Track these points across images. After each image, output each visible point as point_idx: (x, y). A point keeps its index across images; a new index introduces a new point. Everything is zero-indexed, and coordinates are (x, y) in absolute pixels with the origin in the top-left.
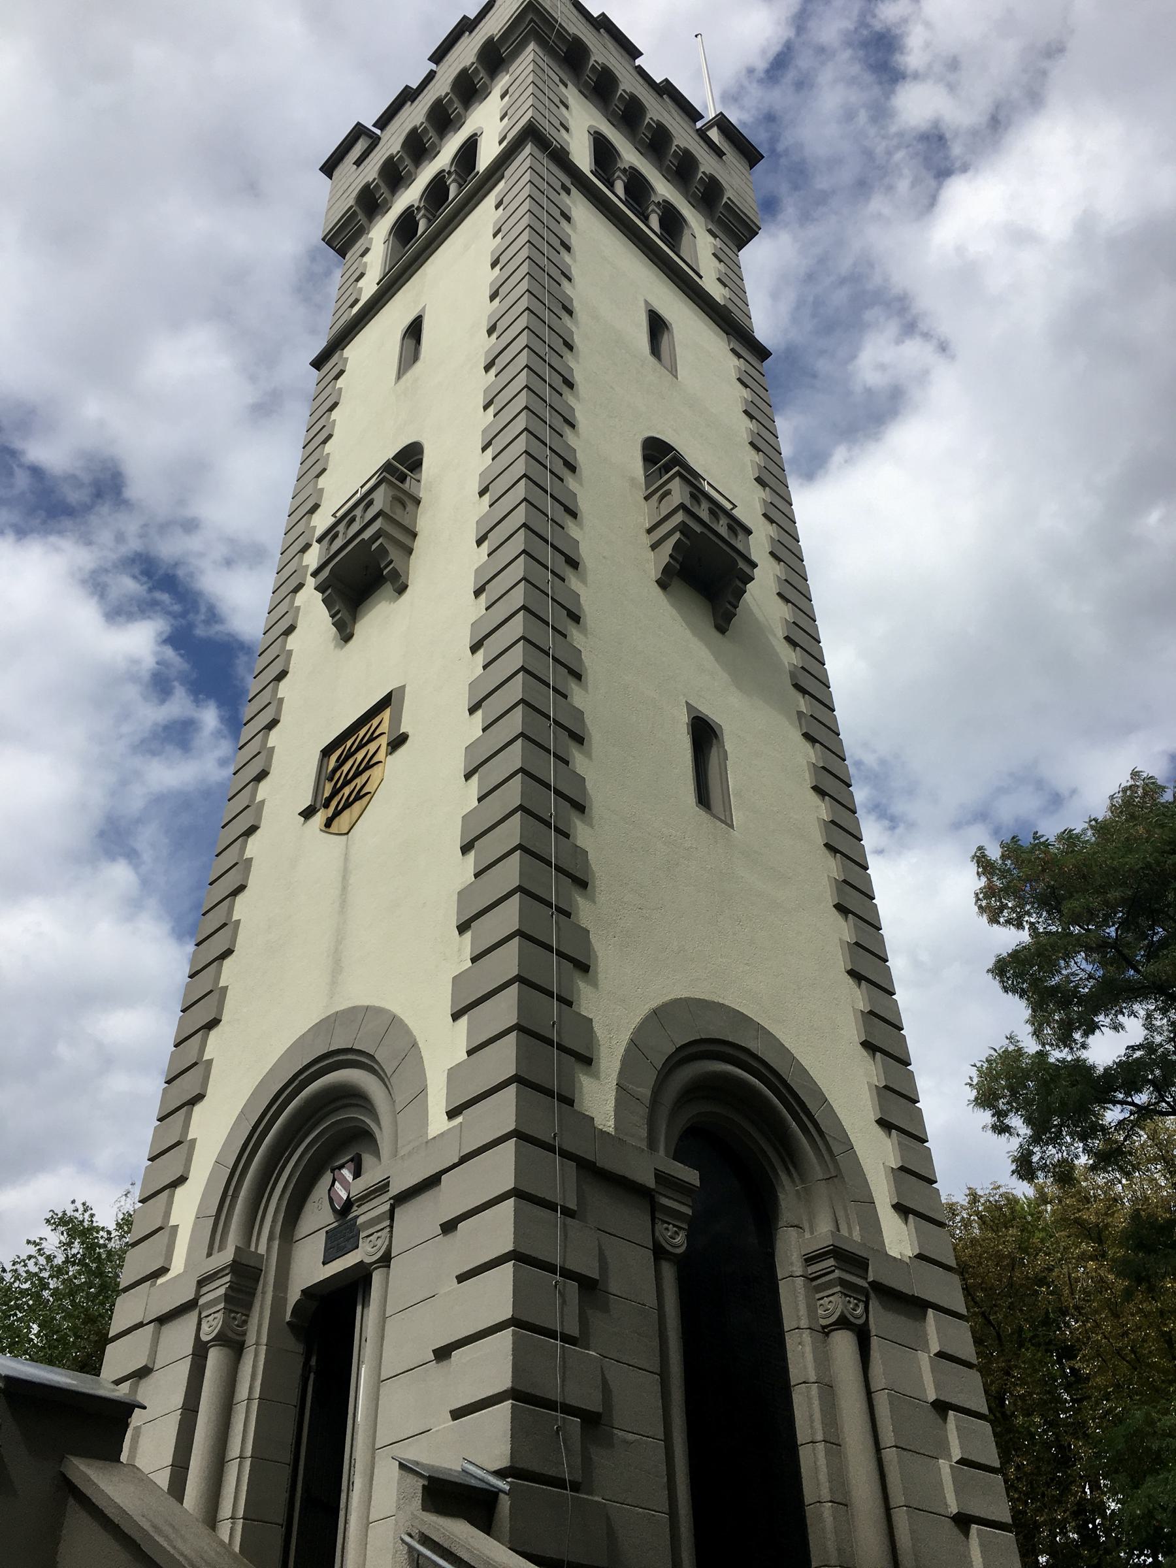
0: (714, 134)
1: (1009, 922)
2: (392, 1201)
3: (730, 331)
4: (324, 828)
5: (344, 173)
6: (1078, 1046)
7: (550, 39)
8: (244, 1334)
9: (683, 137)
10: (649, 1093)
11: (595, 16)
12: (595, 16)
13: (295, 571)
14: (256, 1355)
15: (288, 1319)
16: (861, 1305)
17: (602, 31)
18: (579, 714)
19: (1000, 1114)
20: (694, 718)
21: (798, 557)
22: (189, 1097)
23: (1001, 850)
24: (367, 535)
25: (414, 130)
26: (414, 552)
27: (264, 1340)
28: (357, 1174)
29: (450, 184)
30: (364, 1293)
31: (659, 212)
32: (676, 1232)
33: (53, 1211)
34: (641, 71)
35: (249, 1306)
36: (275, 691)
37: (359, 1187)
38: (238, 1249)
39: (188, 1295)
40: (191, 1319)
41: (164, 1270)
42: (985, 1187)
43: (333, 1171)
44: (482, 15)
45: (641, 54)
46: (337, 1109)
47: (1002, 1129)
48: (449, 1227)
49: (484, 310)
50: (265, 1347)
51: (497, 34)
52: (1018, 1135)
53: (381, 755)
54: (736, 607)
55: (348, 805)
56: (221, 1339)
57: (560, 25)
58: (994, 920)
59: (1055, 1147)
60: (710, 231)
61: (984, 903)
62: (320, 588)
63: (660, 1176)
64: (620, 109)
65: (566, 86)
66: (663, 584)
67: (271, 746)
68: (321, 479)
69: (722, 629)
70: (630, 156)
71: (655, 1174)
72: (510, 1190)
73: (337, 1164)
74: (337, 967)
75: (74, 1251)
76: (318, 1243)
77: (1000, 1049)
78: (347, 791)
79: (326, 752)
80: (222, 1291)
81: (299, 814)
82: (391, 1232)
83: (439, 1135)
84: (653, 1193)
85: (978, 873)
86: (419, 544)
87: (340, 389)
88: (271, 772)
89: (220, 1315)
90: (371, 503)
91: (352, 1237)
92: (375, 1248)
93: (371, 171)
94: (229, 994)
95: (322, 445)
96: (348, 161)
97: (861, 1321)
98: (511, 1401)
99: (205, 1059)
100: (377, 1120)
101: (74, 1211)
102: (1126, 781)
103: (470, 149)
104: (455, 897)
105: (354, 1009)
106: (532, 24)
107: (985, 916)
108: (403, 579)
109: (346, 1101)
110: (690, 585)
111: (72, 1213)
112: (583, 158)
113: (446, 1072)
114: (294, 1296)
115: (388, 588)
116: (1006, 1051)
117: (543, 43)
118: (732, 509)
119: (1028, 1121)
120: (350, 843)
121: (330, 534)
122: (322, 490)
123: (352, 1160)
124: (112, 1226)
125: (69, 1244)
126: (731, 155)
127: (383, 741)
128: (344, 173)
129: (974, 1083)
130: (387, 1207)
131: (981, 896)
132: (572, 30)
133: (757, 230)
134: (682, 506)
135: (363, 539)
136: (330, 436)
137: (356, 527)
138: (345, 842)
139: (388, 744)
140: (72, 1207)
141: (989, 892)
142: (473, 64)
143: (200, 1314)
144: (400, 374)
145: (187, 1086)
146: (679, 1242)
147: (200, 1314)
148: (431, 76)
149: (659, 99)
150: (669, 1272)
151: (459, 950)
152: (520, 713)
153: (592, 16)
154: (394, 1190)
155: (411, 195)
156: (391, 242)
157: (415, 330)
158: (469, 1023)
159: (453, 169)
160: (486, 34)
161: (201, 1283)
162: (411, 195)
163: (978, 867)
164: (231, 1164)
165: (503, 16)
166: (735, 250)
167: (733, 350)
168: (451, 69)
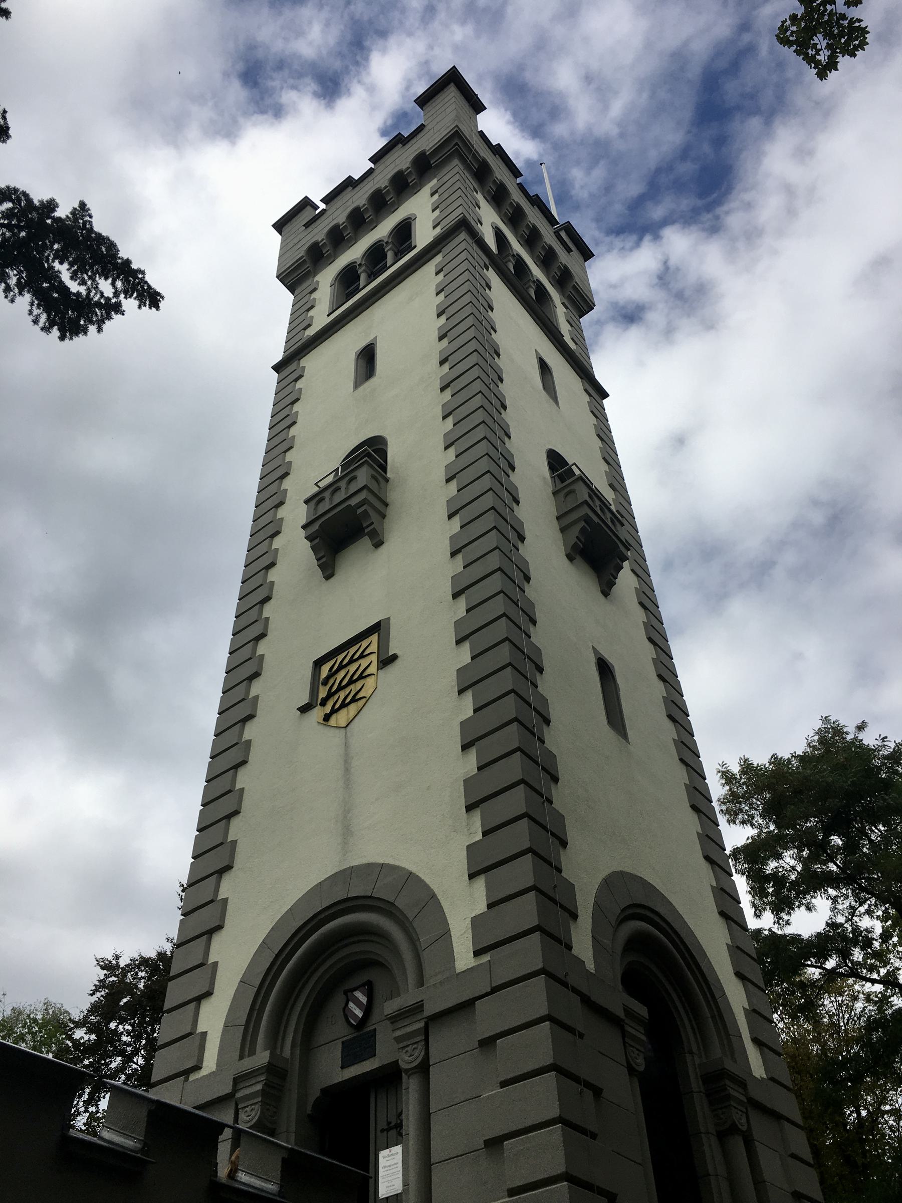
0: (563, 234)
1: (743, 822)
2: (426, 1020)
5: (293, 230)
6: (784, 923)
13: (271, 522)
16: (744, 1115)
17: (497, 156)
22: (208, 928)
24: (354, 502)
29: (387, 251)
31: (534, 287)
36: (261, 612)
39: (227, 1089)
41: (197, 1068)
44: (415, 134)
46: (346, 946)
48: (487, 1043)
51: (428, 150)
55: (344, 705)
57: (475, 150)
64: (510, 213)
65: (477, 193)
66: (570, 558)
68: (288, 454)
71: (624, 1008)
73: (347, 986)
74: (347, 832)
76: (337, 1052)
79: (318, 664)
80: (259, 1087)
81: (297, 709)
86: (390, 512)
89: (257, 1107)
90: (355, 478)
94: (240, 848)
95: (287, 429)
102: (819, 725)
103: (404, 231)
105: (369, 866)
106: (457, 146)
108: (381, 537)
109: (361, 938)
114: (315, 1093)
115: (366, 542)
117: (463, 160)
120: (349, 735)
123: (363, 985)
126: (575, 253)
127: (374, 658)
128: (293, 230)
130: (421, 1025)
133: (593, 306)
134: (365, 487)
135: (350, 505)
142: (408, 168)
143: (237, 1105)
147: (237, 1105)
148: (370, 172)
149: (532, 207)
153: (491, 144)
154: (430, 1009)
155: (355, 253)
159: (390, 241)
160: (419, 148)
162: (355, 253)
166: (578, 318)
167: (586, 390)
168: (389, 168)
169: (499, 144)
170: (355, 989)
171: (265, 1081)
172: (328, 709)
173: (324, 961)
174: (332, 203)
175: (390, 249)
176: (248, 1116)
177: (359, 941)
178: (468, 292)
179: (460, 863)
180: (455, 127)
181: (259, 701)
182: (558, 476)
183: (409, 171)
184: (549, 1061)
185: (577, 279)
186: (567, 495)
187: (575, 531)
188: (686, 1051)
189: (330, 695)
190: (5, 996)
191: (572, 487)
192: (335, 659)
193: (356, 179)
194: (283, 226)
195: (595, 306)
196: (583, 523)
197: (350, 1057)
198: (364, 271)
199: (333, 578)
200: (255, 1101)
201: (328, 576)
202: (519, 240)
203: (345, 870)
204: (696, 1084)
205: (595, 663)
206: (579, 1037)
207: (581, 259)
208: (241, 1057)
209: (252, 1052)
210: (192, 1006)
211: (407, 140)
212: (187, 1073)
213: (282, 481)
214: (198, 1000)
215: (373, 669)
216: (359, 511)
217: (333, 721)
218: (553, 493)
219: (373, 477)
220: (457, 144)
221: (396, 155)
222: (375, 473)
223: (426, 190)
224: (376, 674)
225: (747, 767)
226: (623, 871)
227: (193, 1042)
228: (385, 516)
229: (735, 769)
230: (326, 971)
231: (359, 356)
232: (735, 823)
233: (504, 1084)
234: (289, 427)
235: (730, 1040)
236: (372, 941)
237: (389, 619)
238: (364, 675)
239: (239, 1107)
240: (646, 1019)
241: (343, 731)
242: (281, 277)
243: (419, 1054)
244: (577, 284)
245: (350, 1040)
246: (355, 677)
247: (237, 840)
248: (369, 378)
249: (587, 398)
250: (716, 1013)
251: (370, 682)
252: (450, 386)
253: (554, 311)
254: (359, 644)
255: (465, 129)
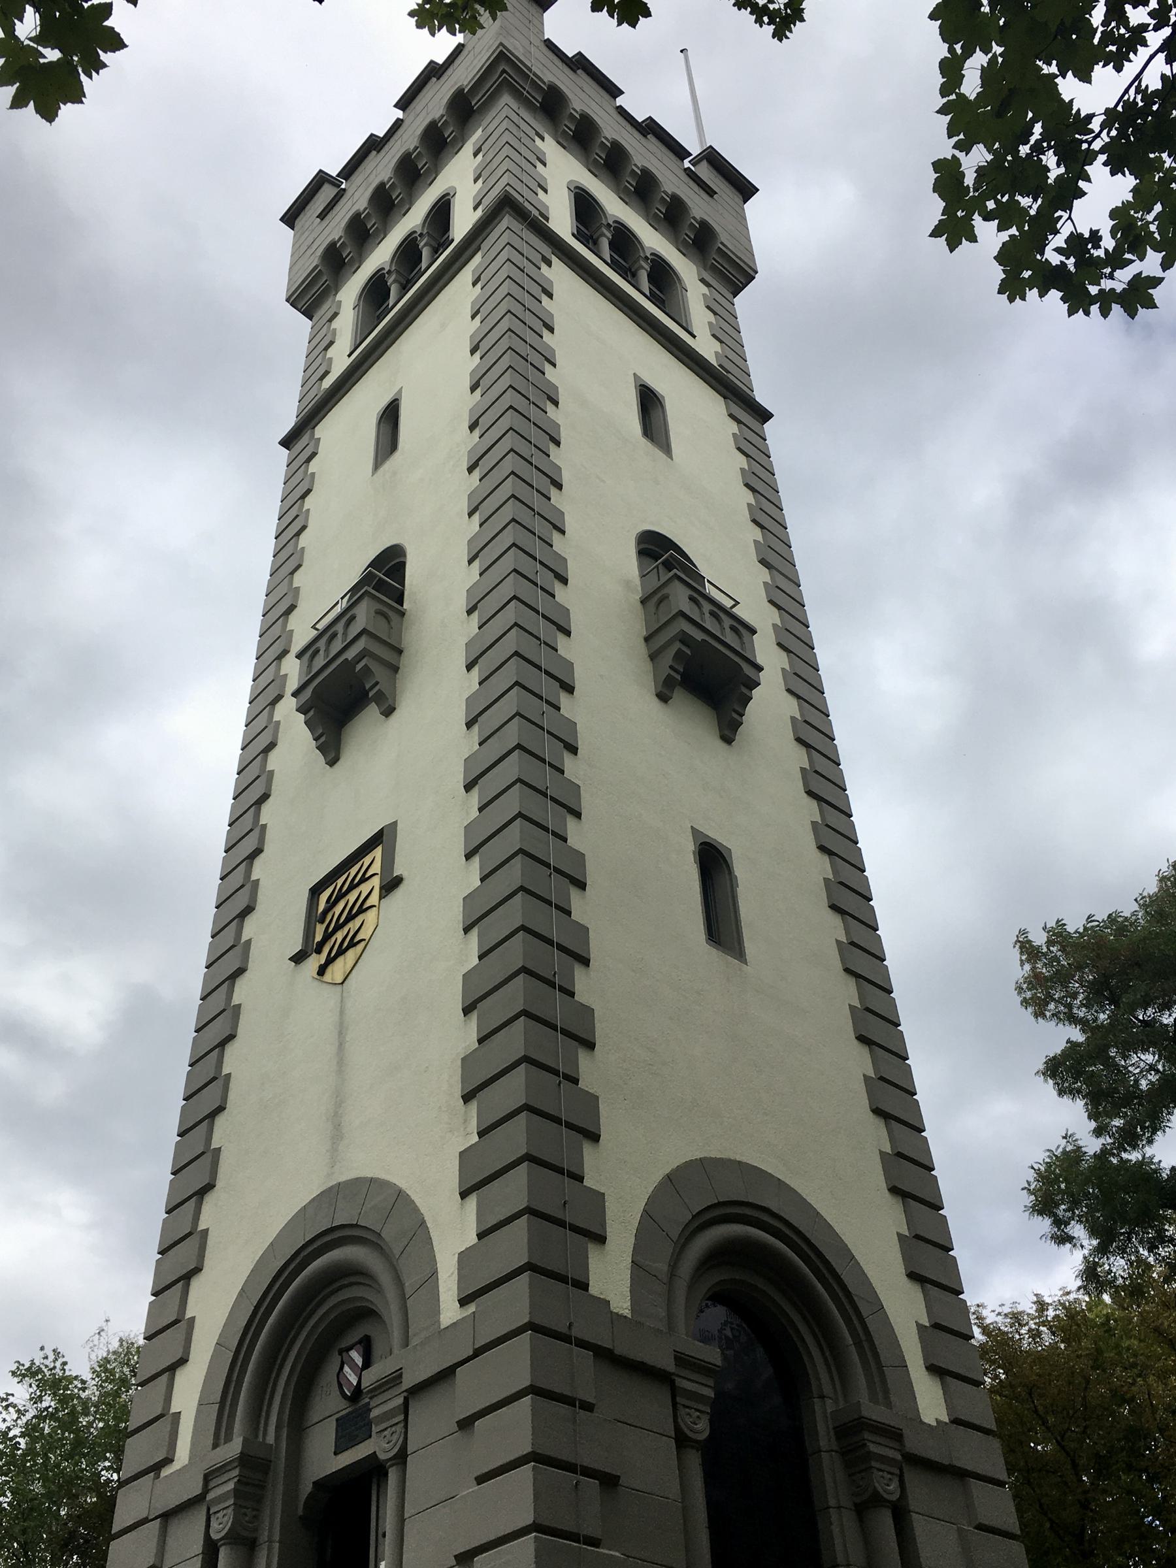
0: (704, 172)
2: (405, 1394)
3: (729, 395)
4: (316, 976)
7: (524, 89)
8: (256, 1530)
9: (671, 180)
10: (665, 1268)
11: (570, 56)
12: (570, 56)
14: (270, 1549)
15: (300, 1512)
17: (580, 71)
18: (580, 857)
19: (1058, 1222)
20: (701, 844)
21: (807, 645)
22: (185, 1271)
23: (1046, 934)
24: (351, 654)
25: (382, 185)
26: (400, 671)
27: (277, 1537)
28: (367, 1364)
30: (379, 1481)
32: (698, 1417)
33: (18, 1362)
34: (621, 111)
35: (259, 1500)
37: (370, 1377)
38: (246, 1442)
40: (198, 1518)
41: (169, 1461)
42: (1053, 1294)
43: (341, 1352)
45: (622, 93)
47: (1063, 1239)
48: (466, 1424)
49: (466, 402)
50: (278, 1544)
51: (467, 85)
52: (1082, 1246)
53: (374, 899)
54: (742, 715)
55: (341, 952)
56: (233, 1538)
57: (535, 74)
58: (1039, 1014)
59: (1123, 1258)
60: (702, 281)
61: (1029, 995)
62: (301, 710)
63: (681, 1360)
65: (543, 139)
66: (663, 698)
67: (256, 878)
69: (728, 740)
70: (614, 206)
72: (526, 1388)
73: (343, 1345)
74: (337, 1132)
75: (45, 1404)
76: (330, 1428)
77: (1057, 1150)
78: (339, 936)
79: (315, 891)
80: (231, 1486)
82: (406, 1427)
83: (451, 1325)
84: (673, 1377)
85: (1021, 960)
86: (404, 660)
87: (313, 474)
88: (257, 908)
89: (230, 1511)
90: (353, 618)
91: (364, 1425)
92: (391, 1444)
93: (335, 228)
94: (224, 1156)
96: (311, 212)
97: (894, 1497)
98: (533, 1463)
99: (199, 1229)
100: (380, 1291)
101: (44, 1358)
103: (442, 212)
104: (459, 1063)
105: (358, 1181)
106: (505, 75)
107: (1030, 1009)
108: (390, 702)
110: (690, 692)
111: (42, 1361)
112: (562, 222)
113: (457, 1255)
114: (307, 1488)
116: (1064, 1152)
117: (517, 94)
118: (734, 606)
119: (1093, 1232)
121: (308, 652)
122: (298, 589)
123: (360, 1342)
124: (87, 1375)
125: (40, 1399)
127: (376, 882)
129: (1032, 1187)
130: (400, 1400)
131: (1025, 986)
132: (548, 77)
134: (364, 632)
136: (304, 528)
137: (337, 645)
138: (340, 994)
139: (381, 888)
140: (42, 1354)
141: (1035, 980)
142: (442, 116)
143: (209, 1509)
144: (377, 465)
145: (183, 1256)
146: (701, 1428)
147: (209, 1509)
148: (398, 124)
149: (643, 139)
150: (694, 1460)
151: (465, 1121)
152: (519, 866)
153: (568, 57)
154: (408, 1381)
155: (381, 255)
156: (361, 307)
157: (391, 415)
158: (478, 1202)
159: (425, 231)
161: (207, 1478)
162: (381, 255)
163: (1022, 953)
164: (234, 1347)
165: (474, 64)
166: (730, 296)
167: (731, 416)
169: (580, 53)
170: (351, 1348)
171: (237, 1478)
172: (323, 957)
173: (313, 1312)
174: (353, 178)
175: (425, 245)
176: (220, 1524)
177: (351, 1284)
178: (507, 313)
179: (450, 1177)
180: (498, 47)
181: (252, 948)
182: (663, 563)
183: (443, 120)
184: (527, 1449)
185: (723, 237)
186: (661, 602)
187: (668, 658)
188: (815, 1396)
189: (327, 936)
190: (109, 1323)
191: (665, 591)
192: (335, 884)
193: (381, 135)
194: (296, 218)
195: (756, 272)
196: (677, 645)
197: (345, 1440)
198: (395, 281)
199: (339, 763)
200: (227, 1504)
201: (332, 762)
202: (622, 196)
203: (331, 1188)
204: (824, 1438)
205: (694, 853)
206: (580, 1408)
207: (738, 198)
208: (215, 1445)
209: (228, 1439)
210: (164, 1378)
211: (444, 68)
212: (157, 1467)
213: (288, 618)
214: (172, 1369)
215: (374, 899)
216: (359, 667)
217: (328, 977)
218: (641, 602)
219: (379, 613)
220: (504, 71)
221: (430, 95)
222: (380, 607)
223: (469, 147)
224: (377, 904)
225: (1058, 935)
226: (705, 1158)
227: (163, 1426)
228: (398, 668)
229: (1039, 938)
230: (321, 1319)
231: (381, 417)
232: (1044, 1017)
233: (481, 1479)
234: (298, 534)
235: (884, 1372)
236: (360, 1283)
237: (395, 824)
238: (365, 907)
239: (211, 1512)
240: (719, 1367)
241: (339, 988)
242: (292, 300)
243: (397, 1439)
244: (724, 245)
245: (347, 1415)
246: (354, 911)
247: (220, 1148)
248: (391, 453)
249: (734, 427)
250: (863, 1338)
251: (370, 916)
252: (478, 465)
253: (682, 296)
254: (361, 862)
255: (518, 48)
